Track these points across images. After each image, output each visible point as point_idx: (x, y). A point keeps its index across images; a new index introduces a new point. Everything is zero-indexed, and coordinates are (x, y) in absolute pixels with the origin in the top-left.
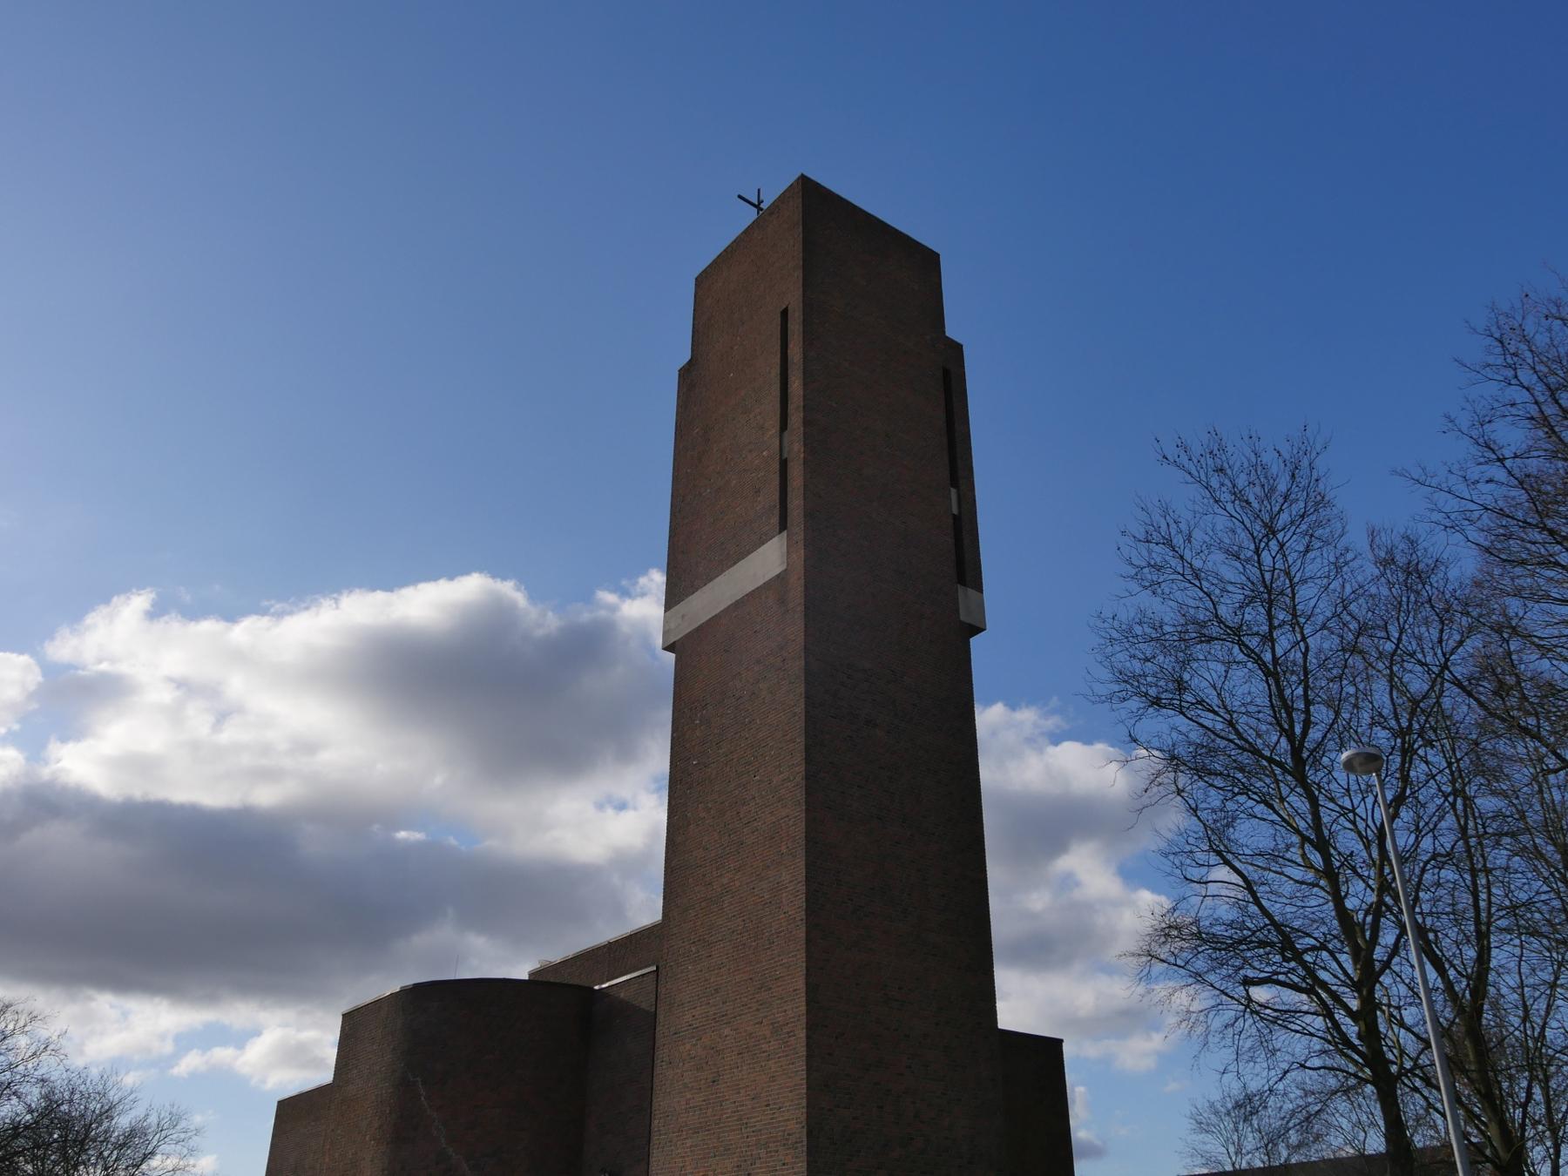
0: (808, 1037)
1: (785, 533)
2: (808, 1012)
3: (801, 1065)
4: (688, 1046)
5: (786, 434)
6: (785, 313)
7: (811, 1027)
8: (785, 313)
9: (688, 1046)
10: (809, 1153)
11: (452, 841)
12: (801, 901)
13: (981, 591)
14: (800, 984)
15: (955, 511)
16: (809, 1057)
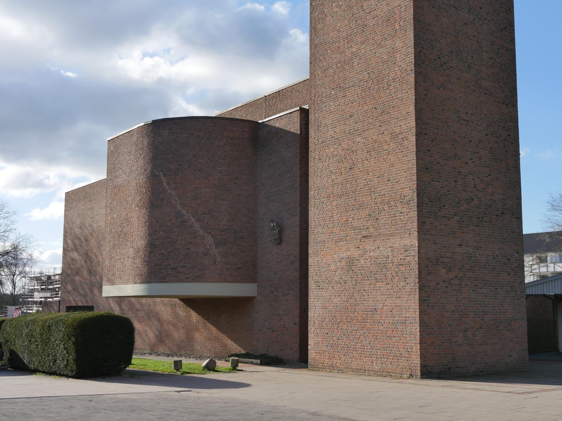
0: (417, 140)
2: (417, 125)
3: (412, 157)
4: (332, 149)
7: (419, 135)
9: (332, 149)
10: (418, 206)
11: (70, 74)
12: (411, 58)
16: (417, 152)
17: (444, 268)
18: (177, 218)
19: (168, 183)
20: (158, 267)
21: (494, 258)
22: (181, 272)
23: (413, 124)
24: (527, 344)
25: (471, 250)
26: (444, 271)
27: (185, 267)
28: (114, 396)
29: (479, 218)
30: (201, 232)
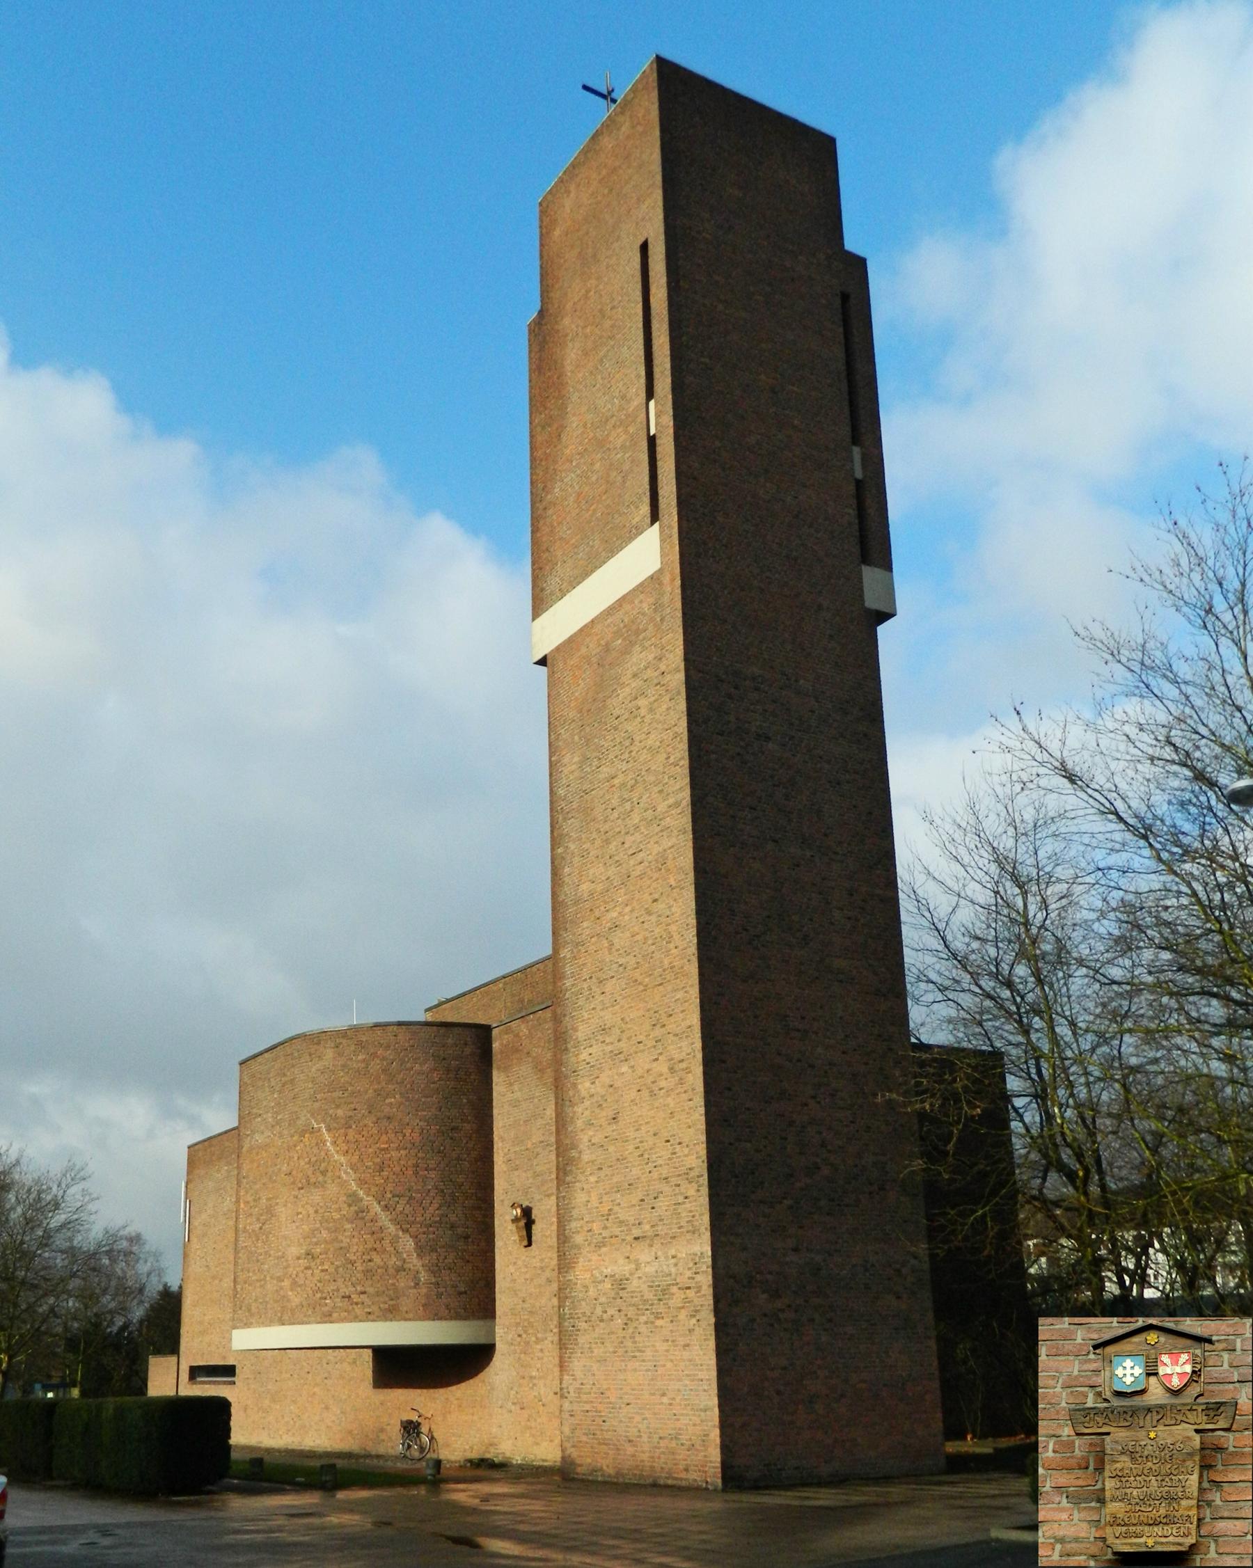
0: (705, 1073)
1: (657, 525)
3: (699, 1100)
5: (449, 1544)
6: (644, 247)
7: (707, 1063)
8: (644, 247)
13: (888, 567)
14: (695, 1019)
15: (859, 474)
17: (763, 1292)
18: (350, 1206)
19: (334, 1143)
20: (319, 1295)
21: (866, 1270)
22: (357, 1304)
23: (698, 1044)
24: (941, 1425)
25: (818, 1258)
26: (765, 1296)
27: (364, 1293)
28: (541, 1564)
29: (833, 1200)
30: (392, 1228)
